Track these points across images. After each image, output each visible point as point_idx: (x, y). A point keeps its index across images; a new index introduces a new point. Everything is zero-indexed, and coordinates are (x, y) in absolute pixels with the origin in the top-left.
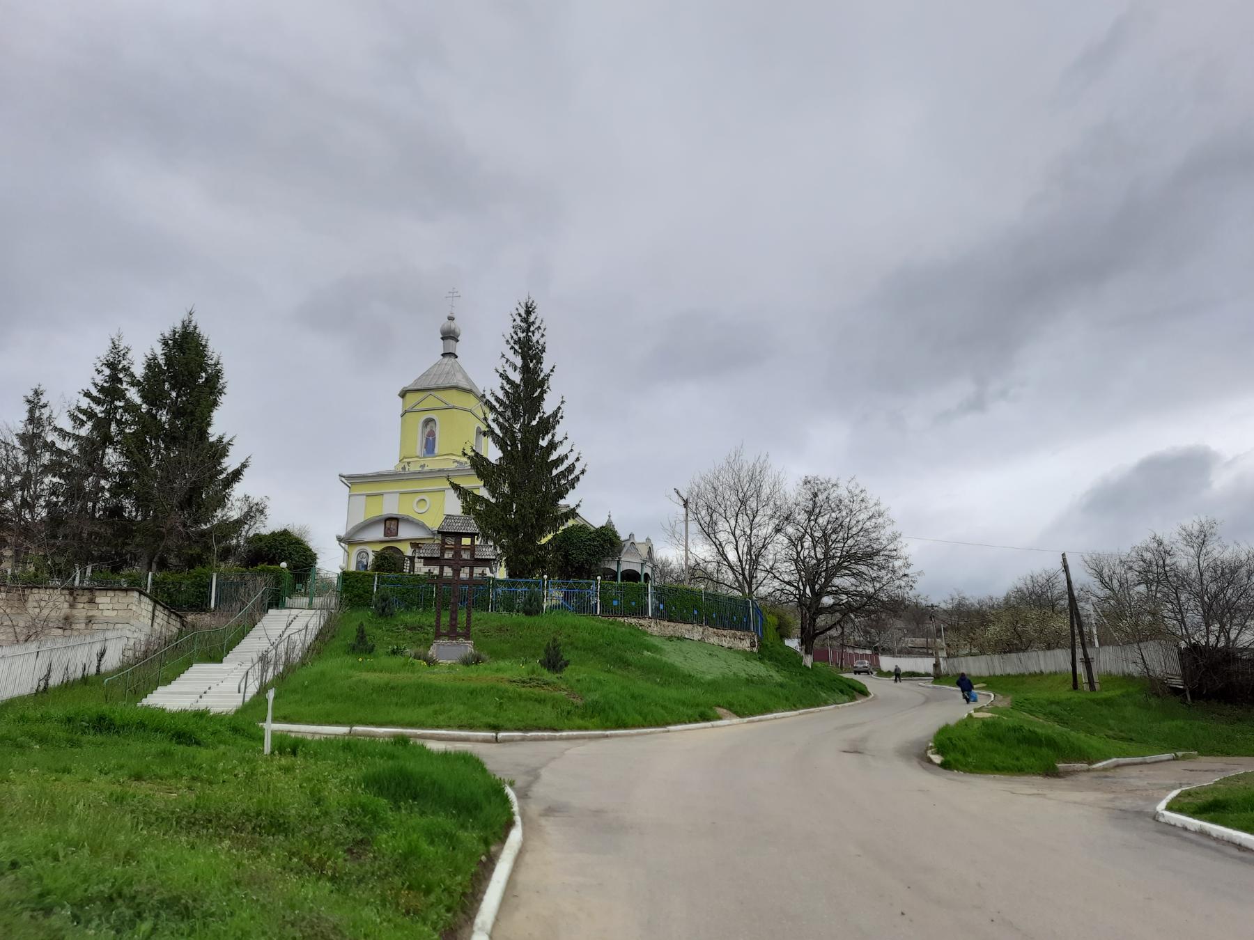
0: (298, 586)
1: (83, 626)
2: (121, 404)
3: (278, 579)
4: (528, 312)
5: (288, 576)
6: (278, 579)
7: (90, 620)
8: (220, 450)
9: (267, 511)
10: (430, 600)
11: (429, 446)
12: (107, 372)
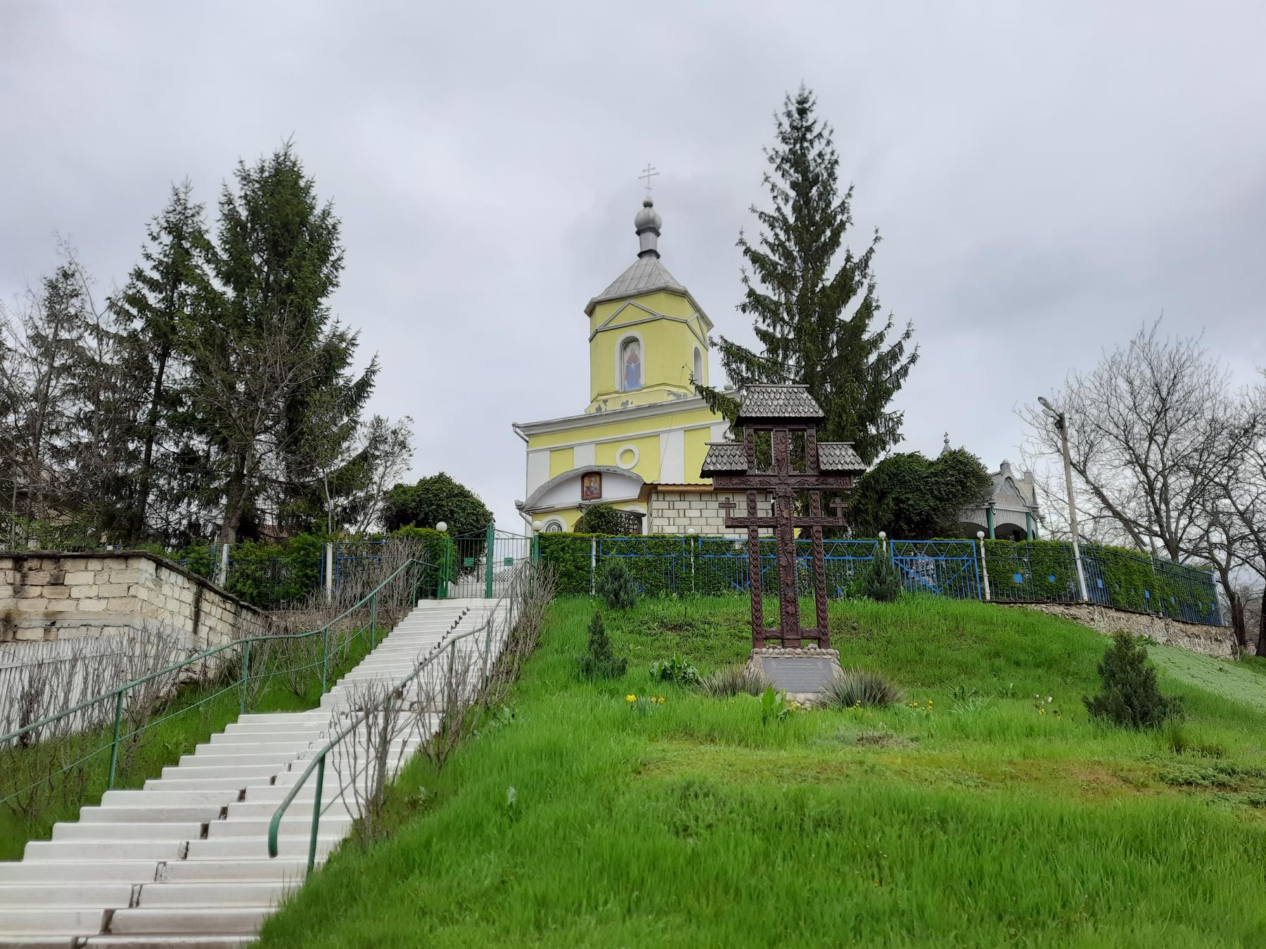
0: (468, 562)
1: (39, 633)
2: (192, 290)
3: (434, 550)
4: (802, 112)
5: (450, 548)
6: (434, 550)
7: (52, 623)
8: (336, 355)
9: (411, 443)
11: (632, 375)
12: (167, 239)
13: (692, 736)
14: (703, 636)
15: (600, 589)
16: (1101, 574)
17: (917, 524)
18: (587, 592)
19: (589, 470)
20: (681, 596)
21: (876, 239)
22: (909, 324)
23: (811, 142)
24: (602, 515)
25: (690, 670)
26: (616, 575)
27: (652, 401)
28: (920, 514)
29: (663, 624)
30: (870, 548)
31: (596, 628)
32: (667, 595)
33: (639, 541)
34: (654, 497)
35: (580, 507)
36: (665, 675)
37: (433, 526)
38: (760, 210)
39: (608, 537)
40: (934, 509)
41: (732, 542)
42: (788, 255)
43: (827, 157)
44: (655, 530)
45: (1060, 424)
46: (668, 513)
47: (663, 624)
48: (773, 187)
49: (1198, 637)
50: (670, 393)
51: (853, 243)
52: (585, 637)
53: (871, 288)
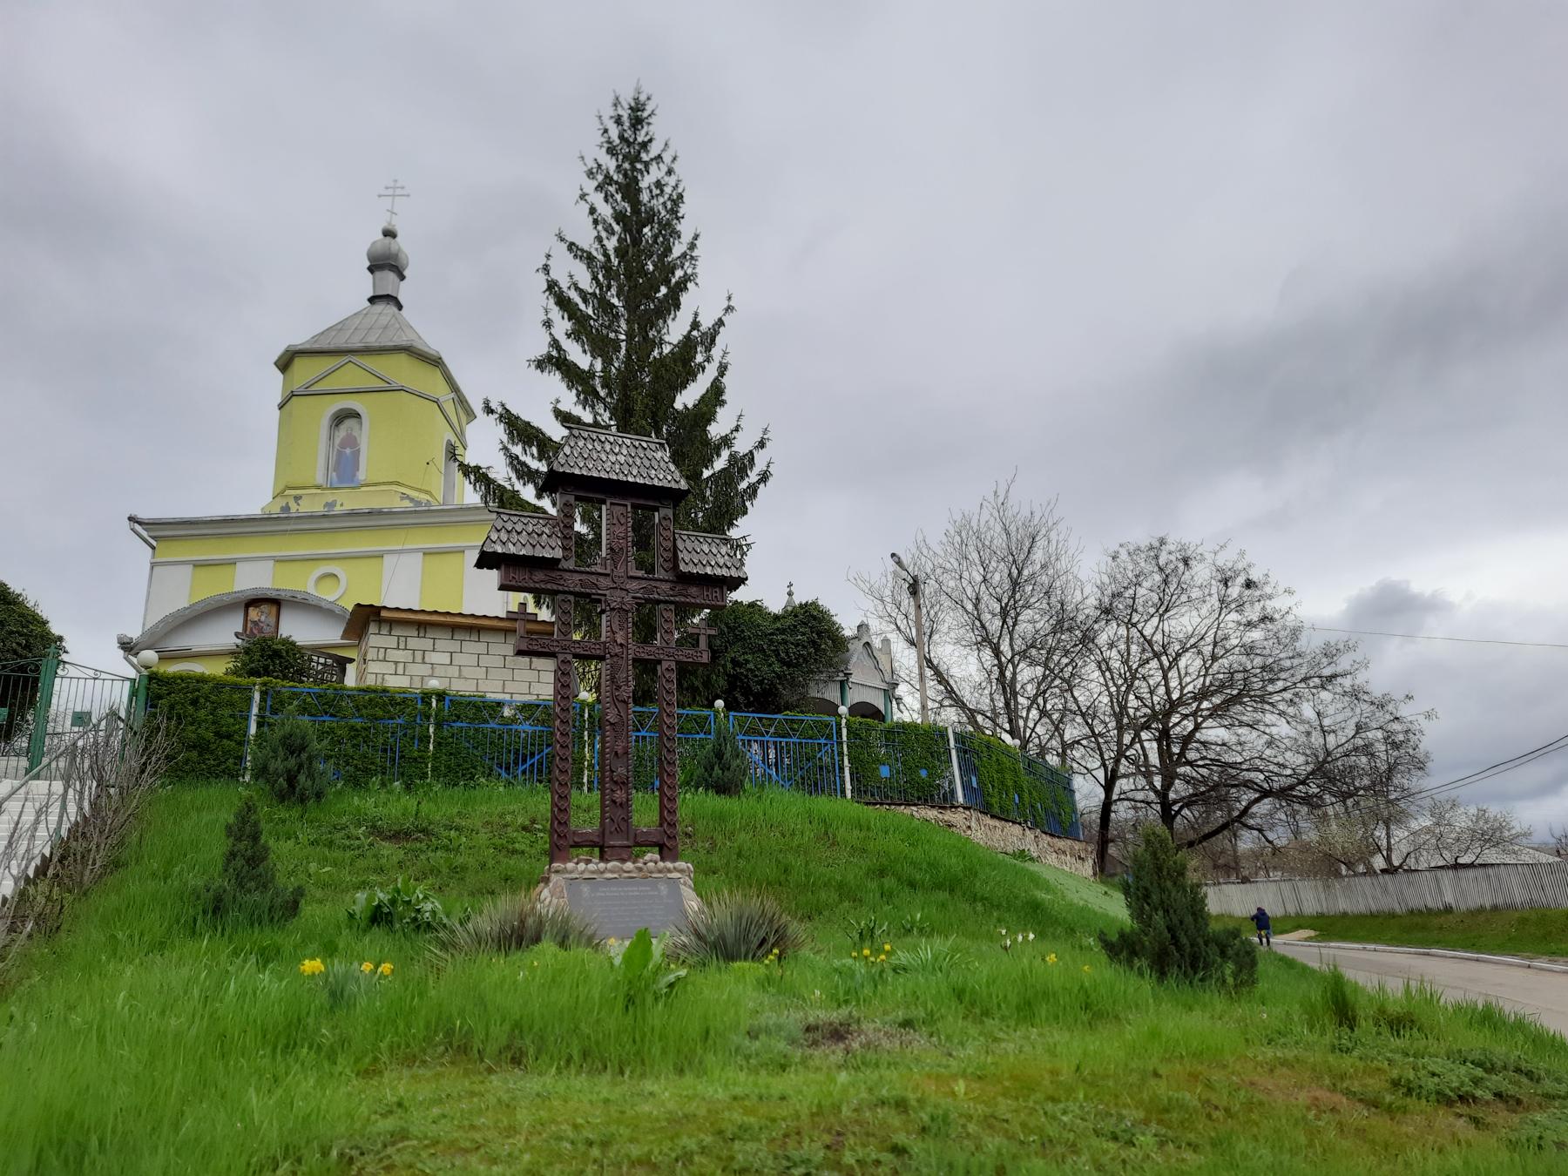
4: (637, 122)
10: (419, 761)
11: (345, 468)
13: (464, 1049)
14: (447, 849)
15: (261, 772)
16: (975, 770)
17: (756, 695)
18: (234, 776)
19: (260, 594)
20: (408, 788)
21: (729, 309)
22: (765, 431)
23: (647, 164)
24: (276, 654)
25: (428, 906)
26: (294, 746)
27: (375, 504)
28: (761, 683)
29: (375, 830)
30: (702, 723)
31: (245, 831)
32: (383, 784)
33: (341, 692)
34: (373, 628)
36: (379, 917)
38: (570, 239)
39: (285, 686)
40: (779, 677)
41: (500, 704)
42: (604, 306)
43: (668, 190)
44: (370, 681)
45: (914, 589)
46: (395, 655)
47: (375, 830)
48: (592, 211)
49: (1064, 853)
50: (405, 497)
51: (700, 304)
52: (217, 847)
53: (723, 369)
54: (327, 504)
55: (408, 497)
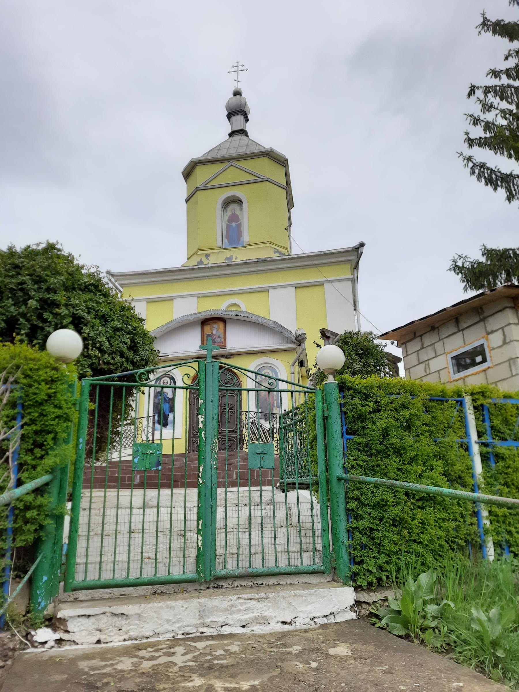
11: (233, 235)
19: (214, 315)
35: (198, 358)
37: (38, 336)
50: (276, 251)
54: (227, 259)
55: (278, 251)
